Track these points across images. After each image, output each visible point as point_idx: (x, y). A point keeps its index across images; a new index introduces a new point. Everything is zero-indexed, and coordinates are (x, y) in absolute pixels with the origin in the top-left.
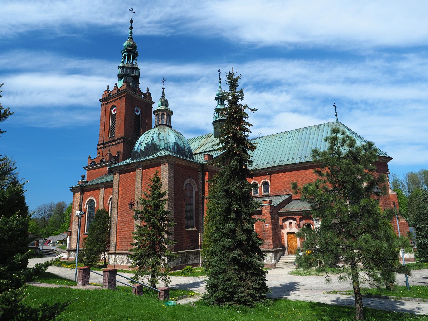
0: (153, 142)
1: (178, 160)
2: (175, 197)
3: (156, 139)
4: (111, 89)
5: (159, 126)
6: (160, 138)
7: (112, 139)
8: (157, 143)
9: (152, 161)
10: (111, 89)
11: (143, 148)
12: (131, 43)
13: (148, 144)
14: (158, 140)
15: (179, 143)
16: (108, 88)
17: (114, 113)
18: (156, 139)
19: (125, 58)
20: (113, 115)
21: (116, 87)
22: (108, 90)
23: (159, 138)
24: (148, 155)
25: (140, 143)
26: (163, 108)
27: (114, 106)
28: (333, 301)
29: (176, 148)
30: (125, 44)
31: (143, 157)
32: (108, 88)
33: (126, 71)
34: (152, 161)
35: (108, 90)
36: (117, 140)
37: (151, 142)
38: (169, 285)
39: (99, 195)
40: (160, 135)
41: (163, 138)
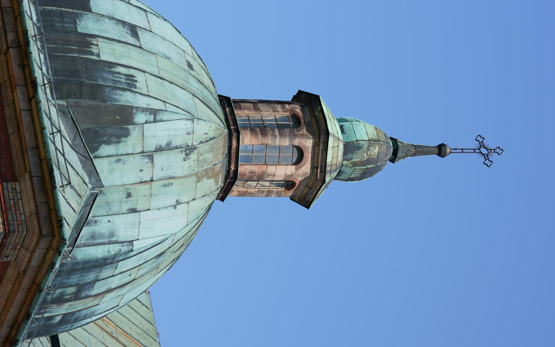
0: (140, 118)
1: (26, 282)
3: (157, 134)
5: (233, 129)
6: (159, 158)
9: (25, 118)
11: (106, 52)
12: (117, 203)
13: (130, 84)
14: (150, 146)
18: (157, 134)
23: (159, 149)
24: (59, 89)
25: (133, 30)
26: (335, 153)
28: (69, 320)
31: (52, 57)
34: (25, 118)
37: (141, 102)
40: (177, 157)
41: (158, 174)
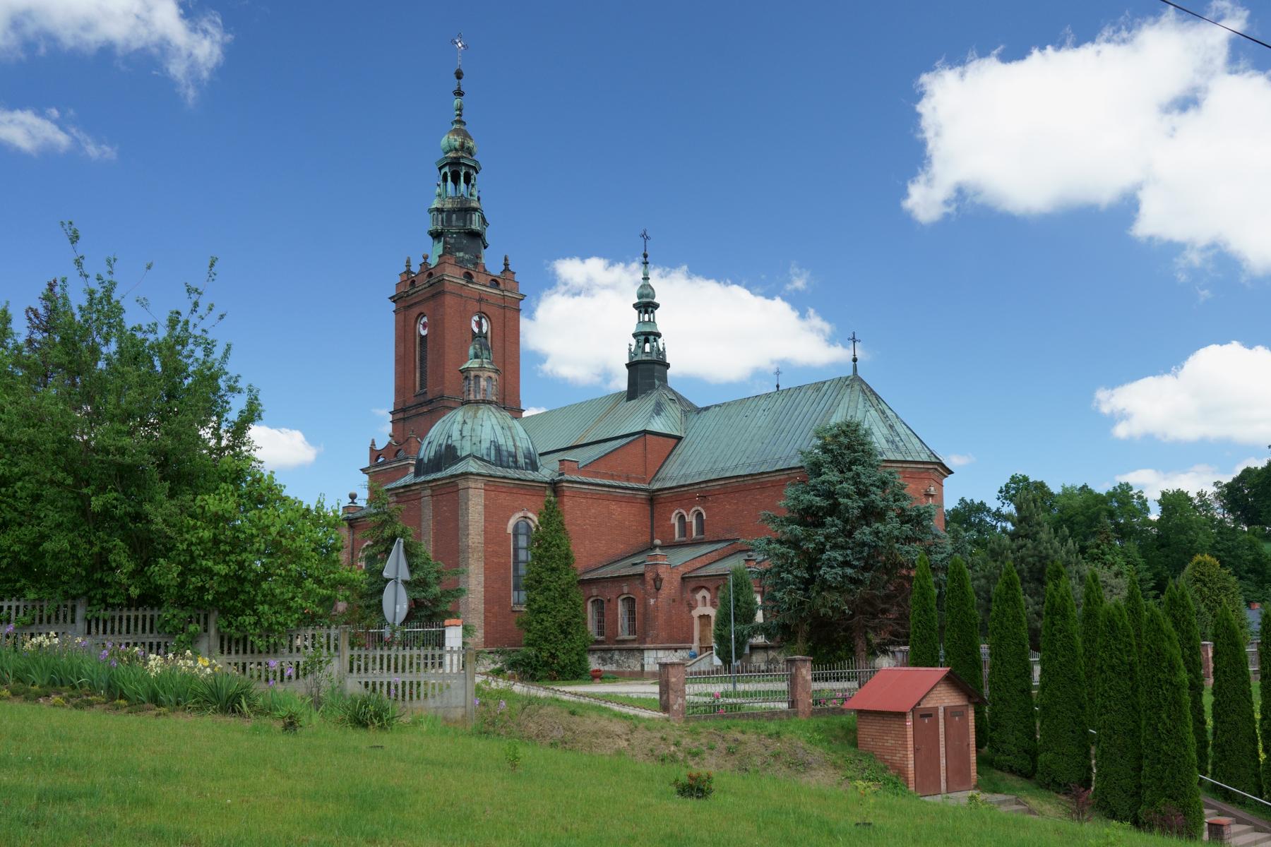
2: (485, 551)
3: (456, 435)
4: (416, 268)
7: (422, 399)
8: (457, 444)
10: (416, 268)
11: (432, 454)
15: (501, 441)
16: (408, 266)
17: (424, 333)
18: (456, 435)
19: (445, 179)
20: (422, 337)
21: (425, 265)
22: (408, 272)
24: (439, 470)
27: (421, 315)
29: (493, 452)
30: (444, 142)
32: (408, 266)
33: (449, 219)
35: (408, 272)
36: (431, 401)
38: (123, 403)
39: (487, 542)
